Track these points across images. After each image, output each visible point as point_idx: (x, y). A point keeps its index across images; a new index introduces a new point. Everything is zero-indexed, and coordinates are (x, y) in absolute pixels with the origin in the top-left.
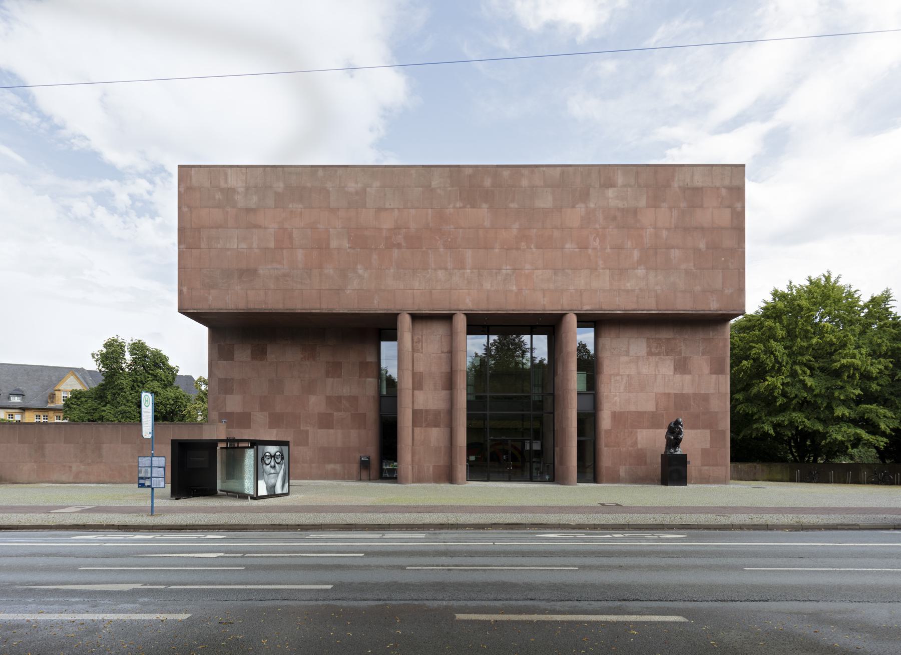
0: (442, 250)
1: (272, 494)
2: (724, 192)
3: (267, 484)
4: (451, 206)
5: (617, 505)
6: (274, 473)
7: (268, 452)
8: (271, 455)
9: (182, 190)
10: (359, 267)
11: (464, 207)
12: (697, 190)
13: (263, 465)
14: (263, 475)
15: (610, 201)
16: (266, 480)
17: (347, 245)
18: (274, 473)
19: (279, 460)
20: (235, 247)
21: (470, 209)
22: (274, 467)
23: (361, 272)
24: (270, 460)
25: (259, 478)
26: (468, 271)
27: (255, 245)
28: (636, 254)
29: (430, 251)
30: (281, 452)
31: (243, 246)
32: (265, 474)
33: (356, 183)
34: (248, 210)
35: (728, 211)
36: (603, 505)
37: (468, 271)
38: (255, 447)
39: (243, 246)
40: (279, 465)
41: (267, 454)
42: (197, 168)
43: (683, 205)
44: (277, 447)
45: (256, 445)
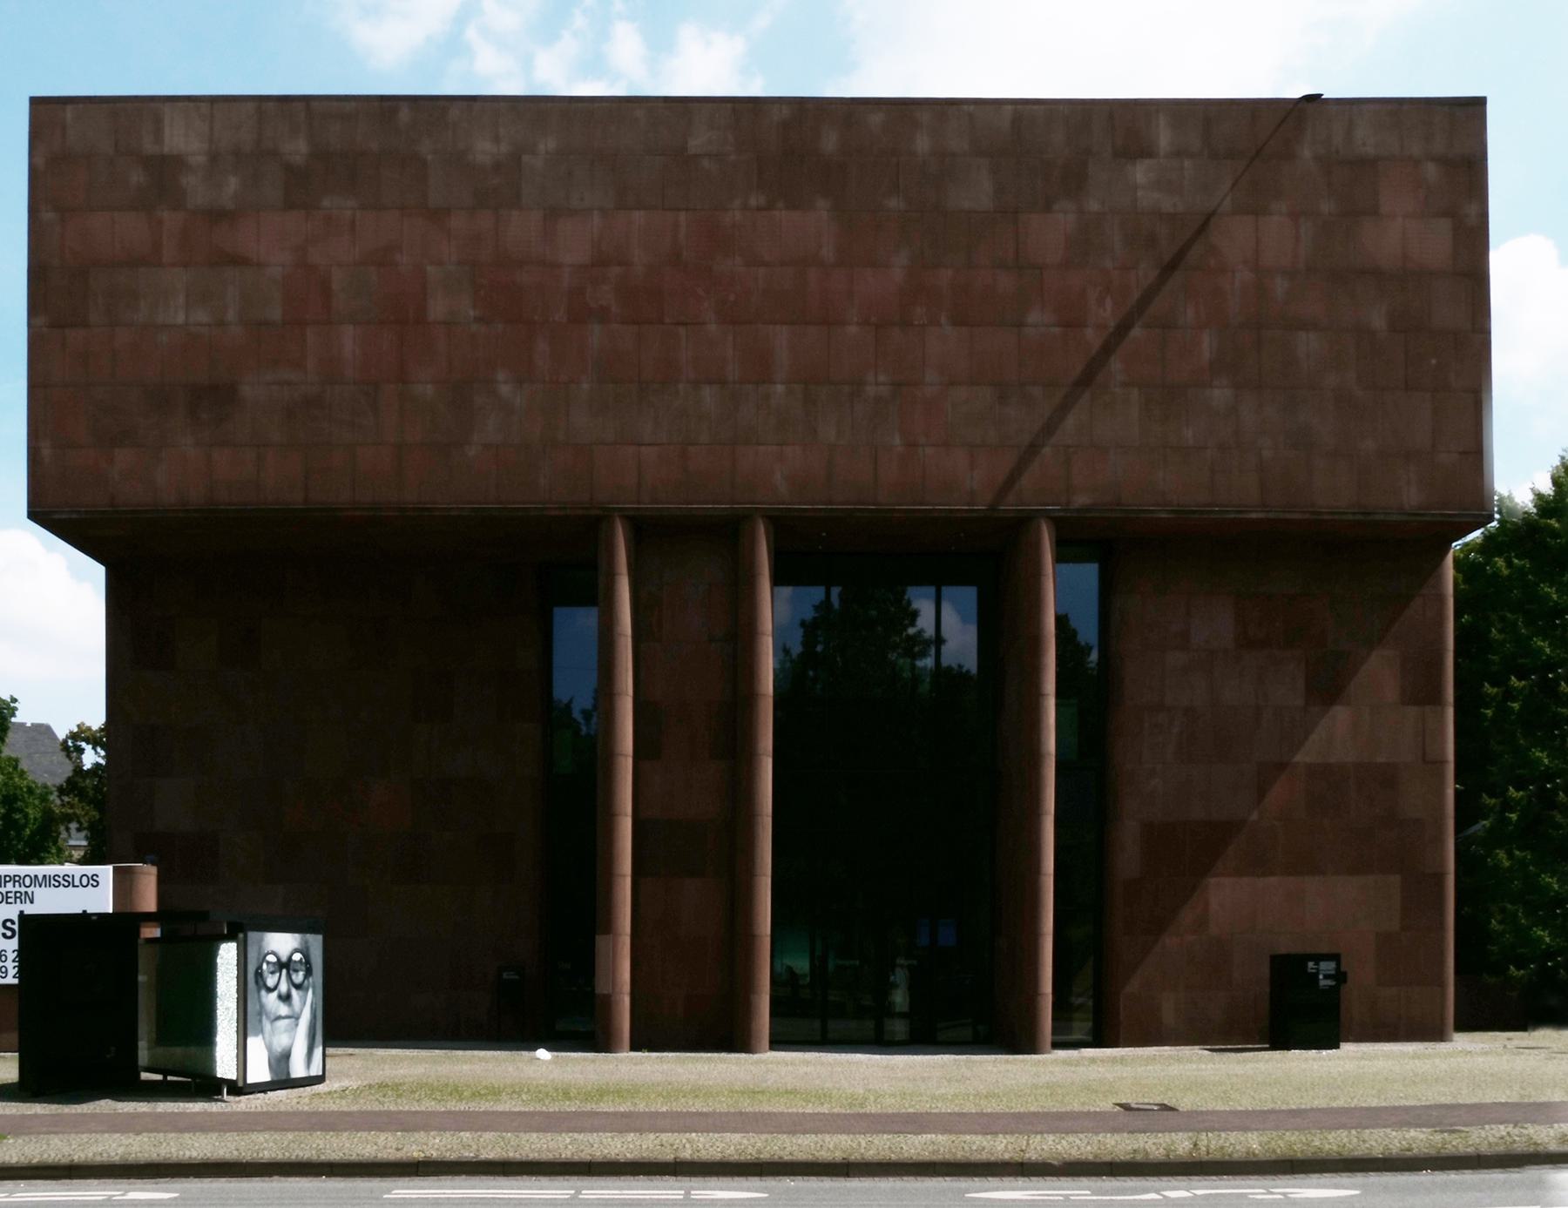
0: (713, 328)
1: (282, 1081)
2: (1431, 171)
3: (269, 1048)
4: (737, 203)
5: (1165, 1108)
6: (287, 1017)
7: (274, 953)
8: (279, 959)
9: (40, 161)
10: (501, 376)
11: (770, 207)
12: (1365, 165)
13: (259, 991)
14: (260, 1021)
15: (1140, 193)
16: (267, 1039)
17: (472, 313)
18: (287, 1017)
19: (299, 977)
20: (181, 319)
21: (783, 212)
22: (286, 998)
23: (505, 390)
24: (278, 974)
25: (249, 1032)
26: (780, 388)
27: (231, 315)
28: (1207, 345)
29: (682, 330)
30: (305, 951)
31: (201, 316)
32: (264, 1017)
33: (497, 139)
34: (217, 216)
35: (1444, 225)
36: (1126, 1107)
37: (780, 388)
38: (241, 936)
39: (201, 316)
40: (301, 993)
41: (271, 958)
42: (81, 106)
43: (1326, 207)
44: (297, 935)
45: (242, 931)
